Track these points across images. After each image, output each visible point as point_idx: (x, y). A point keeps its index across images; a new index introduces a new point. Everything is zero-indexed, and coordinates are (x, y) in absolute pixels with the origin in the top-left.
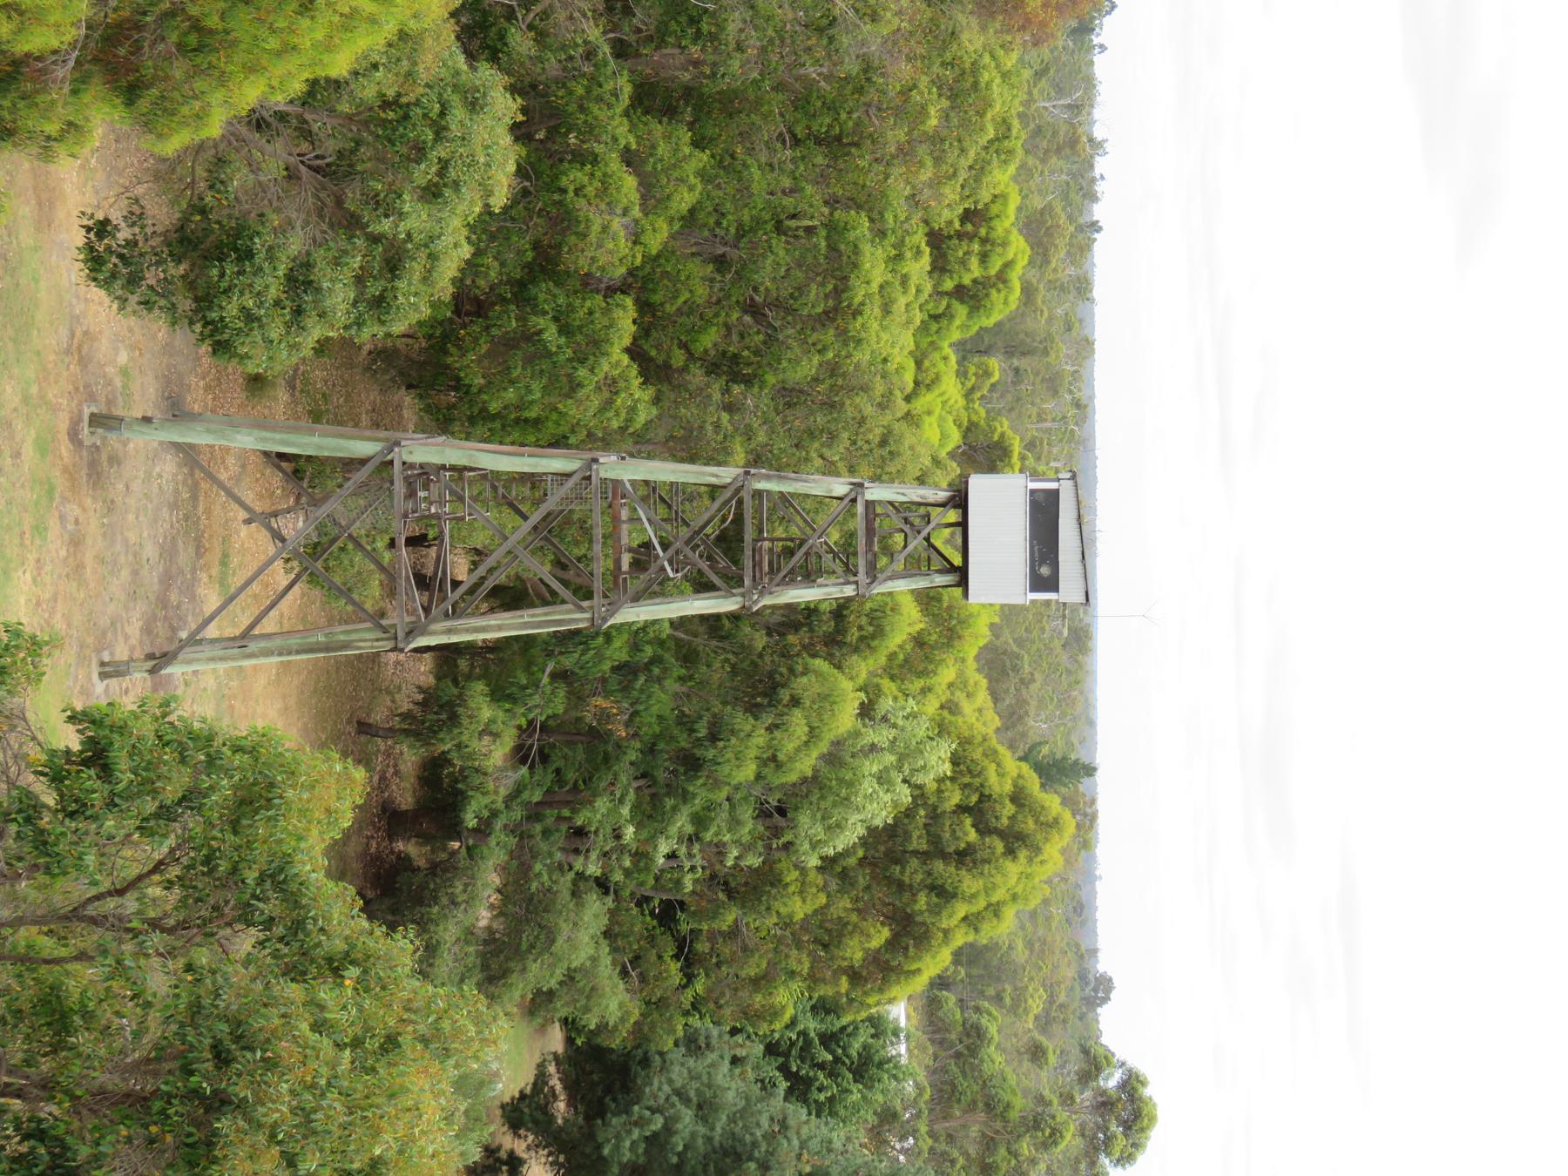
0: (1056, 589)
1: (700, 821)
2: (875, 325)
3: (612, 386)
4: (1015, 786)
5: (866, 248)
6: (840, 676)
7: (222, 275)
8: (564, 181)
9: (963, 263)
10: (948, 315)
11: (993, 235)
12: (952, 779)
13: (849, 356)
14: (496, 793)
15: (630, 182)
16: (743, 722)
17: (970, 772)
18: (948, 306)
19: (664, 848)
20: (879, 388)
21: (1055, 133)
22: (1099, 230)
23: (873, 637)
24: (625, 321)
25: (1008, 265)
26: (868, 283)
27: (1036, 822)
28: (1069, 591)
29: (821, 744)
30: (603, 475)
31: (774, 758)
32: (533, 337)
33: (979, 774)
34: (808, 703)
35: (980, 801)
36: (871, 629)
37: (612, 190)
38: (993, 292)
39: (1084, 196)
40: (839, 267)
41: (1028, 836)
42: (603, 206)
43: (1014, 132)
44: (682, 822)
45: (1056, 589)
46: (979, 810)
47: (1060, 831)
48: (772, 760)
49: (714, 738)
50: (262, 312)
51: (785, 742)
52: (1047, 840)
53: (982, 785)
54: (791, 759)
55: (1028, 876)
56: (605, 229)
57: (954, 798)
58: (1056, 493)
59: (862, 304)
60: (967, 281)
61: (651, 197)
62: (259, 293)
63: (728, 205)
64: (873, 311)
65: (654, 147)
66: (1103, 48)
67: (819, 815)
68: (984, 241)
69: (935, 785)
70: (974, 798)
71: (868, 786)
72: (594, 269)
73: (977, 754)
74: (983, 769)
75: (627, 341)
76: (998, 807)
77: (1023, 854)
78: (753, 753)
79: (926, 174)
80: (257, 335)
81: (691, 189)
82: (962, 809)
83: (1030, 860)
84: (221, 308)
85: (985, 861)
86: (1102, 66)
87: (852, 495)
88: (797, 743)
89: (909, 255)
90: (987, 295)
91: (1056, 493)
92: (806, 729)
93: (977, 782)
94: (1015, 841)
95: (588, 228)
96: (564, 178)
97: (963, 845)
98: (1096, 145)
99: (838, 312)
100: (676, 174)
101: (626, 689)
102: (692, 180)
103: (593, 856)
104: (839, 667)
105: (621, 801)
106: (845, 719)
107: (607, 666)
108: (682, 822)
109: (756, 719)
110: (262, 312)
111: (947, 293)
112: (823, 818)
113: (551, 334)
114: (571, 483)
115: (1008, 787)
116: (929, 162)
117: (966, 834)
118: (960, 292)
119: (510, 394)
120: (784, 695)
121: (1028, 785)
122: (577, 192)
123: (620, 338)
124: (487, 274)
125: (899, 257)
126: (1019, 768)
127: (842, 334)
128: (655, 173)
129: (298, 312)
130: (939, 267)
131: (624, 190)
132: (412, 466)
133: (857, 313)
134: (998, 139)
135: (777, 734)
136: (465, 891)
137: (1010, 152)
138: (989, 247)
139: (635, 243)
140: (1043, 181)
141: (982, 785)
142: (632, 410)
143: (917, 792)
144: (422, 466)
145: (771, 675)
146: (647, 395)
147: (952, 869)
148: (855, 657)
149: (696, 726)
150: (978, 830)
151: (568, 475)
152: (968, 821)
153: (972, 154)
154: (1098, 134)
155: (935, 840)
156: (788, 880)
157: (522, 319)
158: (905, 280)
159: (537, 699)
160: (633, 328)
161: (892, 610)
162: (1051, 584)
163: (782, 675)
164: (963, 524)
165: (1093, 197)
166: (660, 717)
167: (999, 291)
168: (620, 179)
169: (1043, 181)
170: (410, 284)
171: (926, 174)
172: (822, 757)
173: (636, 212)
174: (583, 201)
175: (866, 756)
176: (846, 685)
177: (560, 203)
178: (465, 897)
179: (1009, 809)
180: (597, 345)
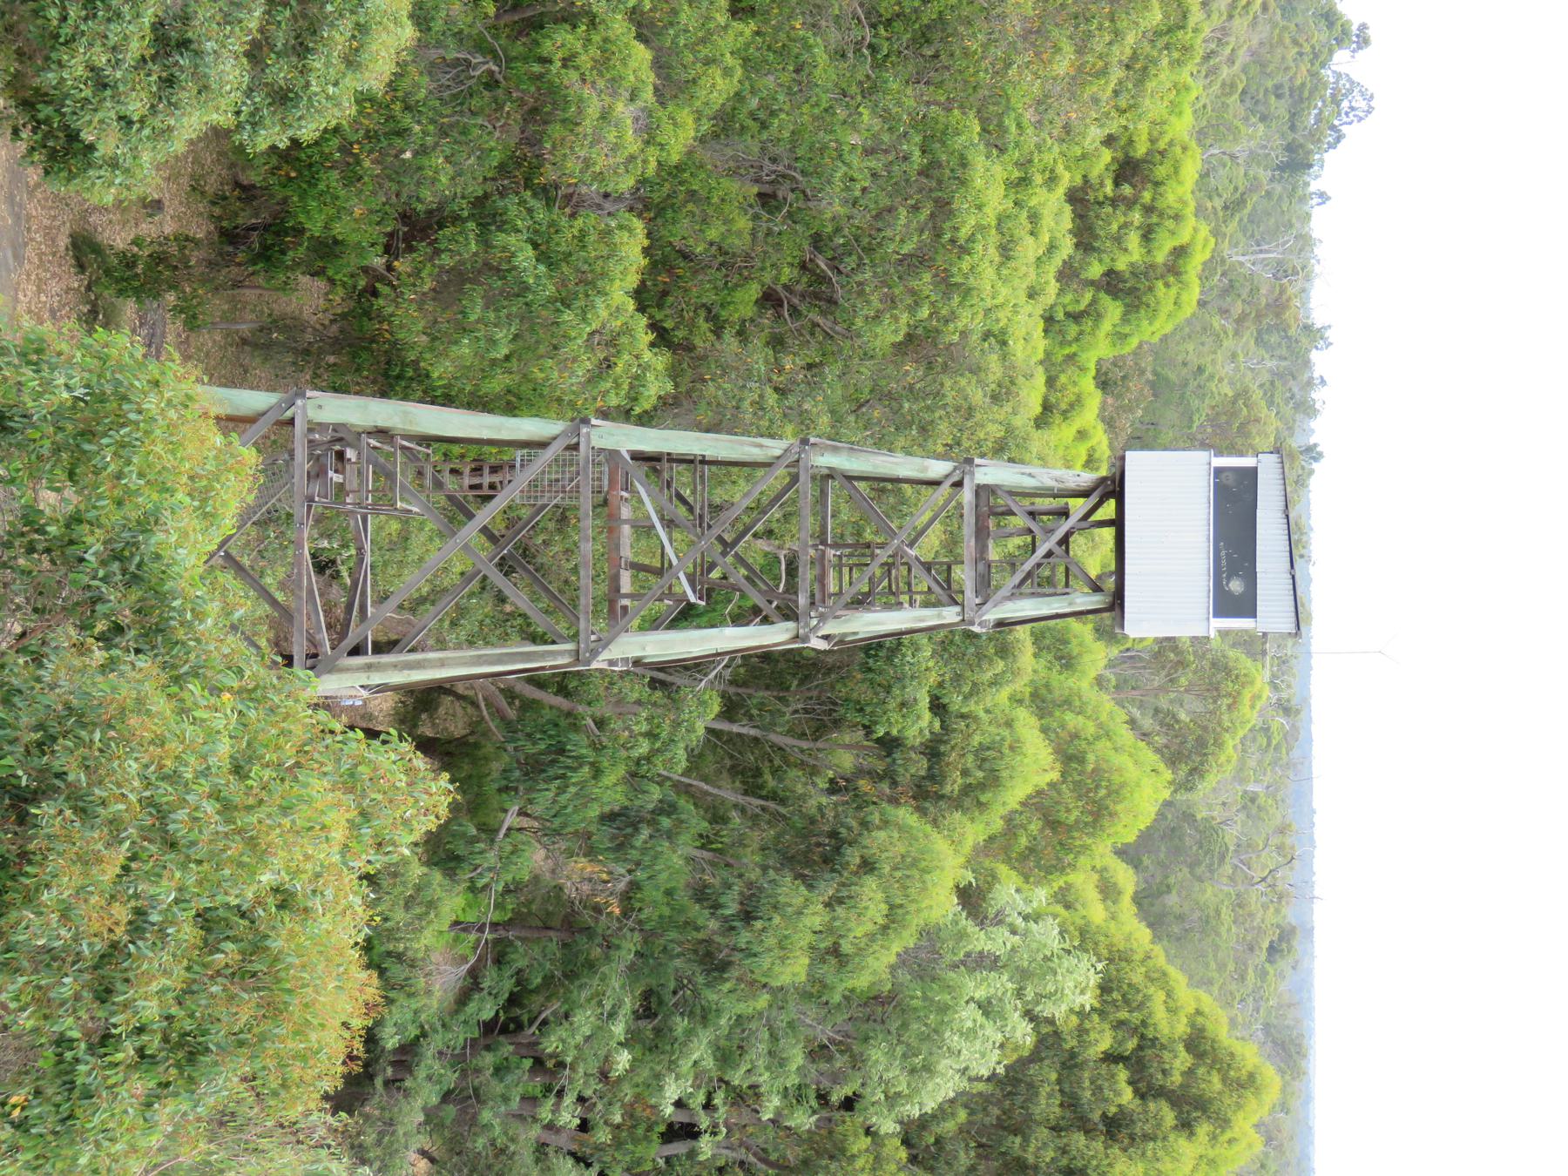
0: (1252, 613)
1: (726, 1056)
2: (989, 272)
3: (610, 342)
4: (1192, 1025)
5: (979, 160)
6: (935, 835)
7: (64, 19)
8: (547, 47)
9: (1118, 240)
10: (1089, 314)
11: (1160, 204)
12: (1102, 1013)
13: (953, 317)
14: (428, 993)
15: (641, 55)
16: (790, 891)
17: (1126, 1001)
18: (1094, 302)
19: (672, 1091)
20: (995, 369)
21: (1254, 291)
22: (1318, 457)
23: (982, 786)
24: (632, 247)
25: (1180, 252)
26: (979, 207)
27: (1224, 1080)
28: (1272, 614)
29: (906, 934)
30: (597, 442)
31: (835, 951)
32: (497, 269)
33: (1141, 1006)
34: (887, 869)
35: (1140, 1047)
36: (980, 774)
37: (615, 61)
38: (1160, 284)
39: (1297, 407)
40: (938, 186)
41: (1210, 1101)
42: (601, 84)
43: (1192, 22)
44: (700, 1051)
45: (1252, 613)
46: (1139, 1057)
47: (1257, 1091)
48: (833, 954)
49: (748, 916)
50: (119, 74)
51: (852, 925)
52: (1239, 1106)
53: (1144, 1023)
54: (860, 951)
55: (1212, 1163)
56: (605, 116)
57: (1104, 1041)
58: (1252, 473)
59: (971, 239)
60: (1121, 265)
61: (672, 84)
62: (114, 49)
63: (781, 97)
64: (986, 251)
65: (675, 12)
66: (1324, 197)
67: (899, 1050)
68: (1149, 210)
69: (1074, 1020)
70: (1131, 1044)
71: (969, 1015)
72: (587, 177)
73: (1137, 977)
74: (1147, 998)
75: (633, 281)
76: (1166, 1055)
77: (1203, 1129)
78: (806, 939)
79: (1063, 65)
80: (109, 112)
81: (727, 72)
82: (1111, 1058)
83: (1214, 1138)
84: (60, 63)
85: (1147, 1137)
86: (1321, 222)
87: (956, 478)
88: (869, 927)
89: (1038, 179)
90: (1151, 289)
91: (1252, 473)
92: (884, 907)
93: (1136, 1018)
94: (1192, 1109)
95: (580, 111)
96: (548, 43)
97: (1113, 1110)
98: (1314, 334)
99: (937, 256)
100: (705, 51)
101: (621, 847)
102: (729, 60)
103: (569, 1099)
104: (935, 823)
105: (612, 1015)
106: (941, 905)
107: (594, 812)
108: (700, 1051)
109: (810, 887)
110: (119, 74)
111: (1092, 283)
112: (905, 1056)
113: (525, 256)
114: (548, 455)
115: (1182, 1028)
116: (1068, 48)
117: (1118, 1094)
118: (1112, 283)
119: (465, 349)
120: (853, 856)
121: (1210, 1027)
122: (566, 62)
123: (624, 272)
124: (434, 181)
125: (1024, 182)
126: (1198, 999)
127: (946, 285)
128: (675, 50)
129: (169, 82)
130: (1086, 239)
131: (633, 64)
132: (322, 427)
133: (964, 250)
134: (1170, 31)
135: (840, 910)
136: (379, 1142)
137: (1186, 49)
138: (1155, 219)
139: (647, 143)
140: (1237, 369)
141: (1144, 1023)
142: (637, 381)
143: (1046, 1029)
144: (337, 427)
145: (834, 834)
146: (659, 361)
147: (1098, 1145)
148: (957, 815)
149: (722, 900)
150: (1136, 1091)
151: (543, 445)
152: (1123, 1074)
153: (1130, 39)
154: (1318, 318)
155: (1071, 1102)
156: (855, 1150)
157: (486, 244)
158: (1034, 218)
159: (491, 858)
160: (644, 262)
161: (1012, 748)
162: (1245, 605)
163: (850, 829)
164: (1118, 523)
165: (1307, 409)
166: (669, 893)
167: (1167, 285)
168: (627, 45)
169: (1237, 369)
170: (327, 65)
171: (1063, 65)
172: (904, 960)
173: (648, 95)
174: (574, 76)
175: (971, 971)
176: (940, 844)
177: (540, 77)
178: (379, 1152)
179: (1181, 1060)
180: (592, 282)
